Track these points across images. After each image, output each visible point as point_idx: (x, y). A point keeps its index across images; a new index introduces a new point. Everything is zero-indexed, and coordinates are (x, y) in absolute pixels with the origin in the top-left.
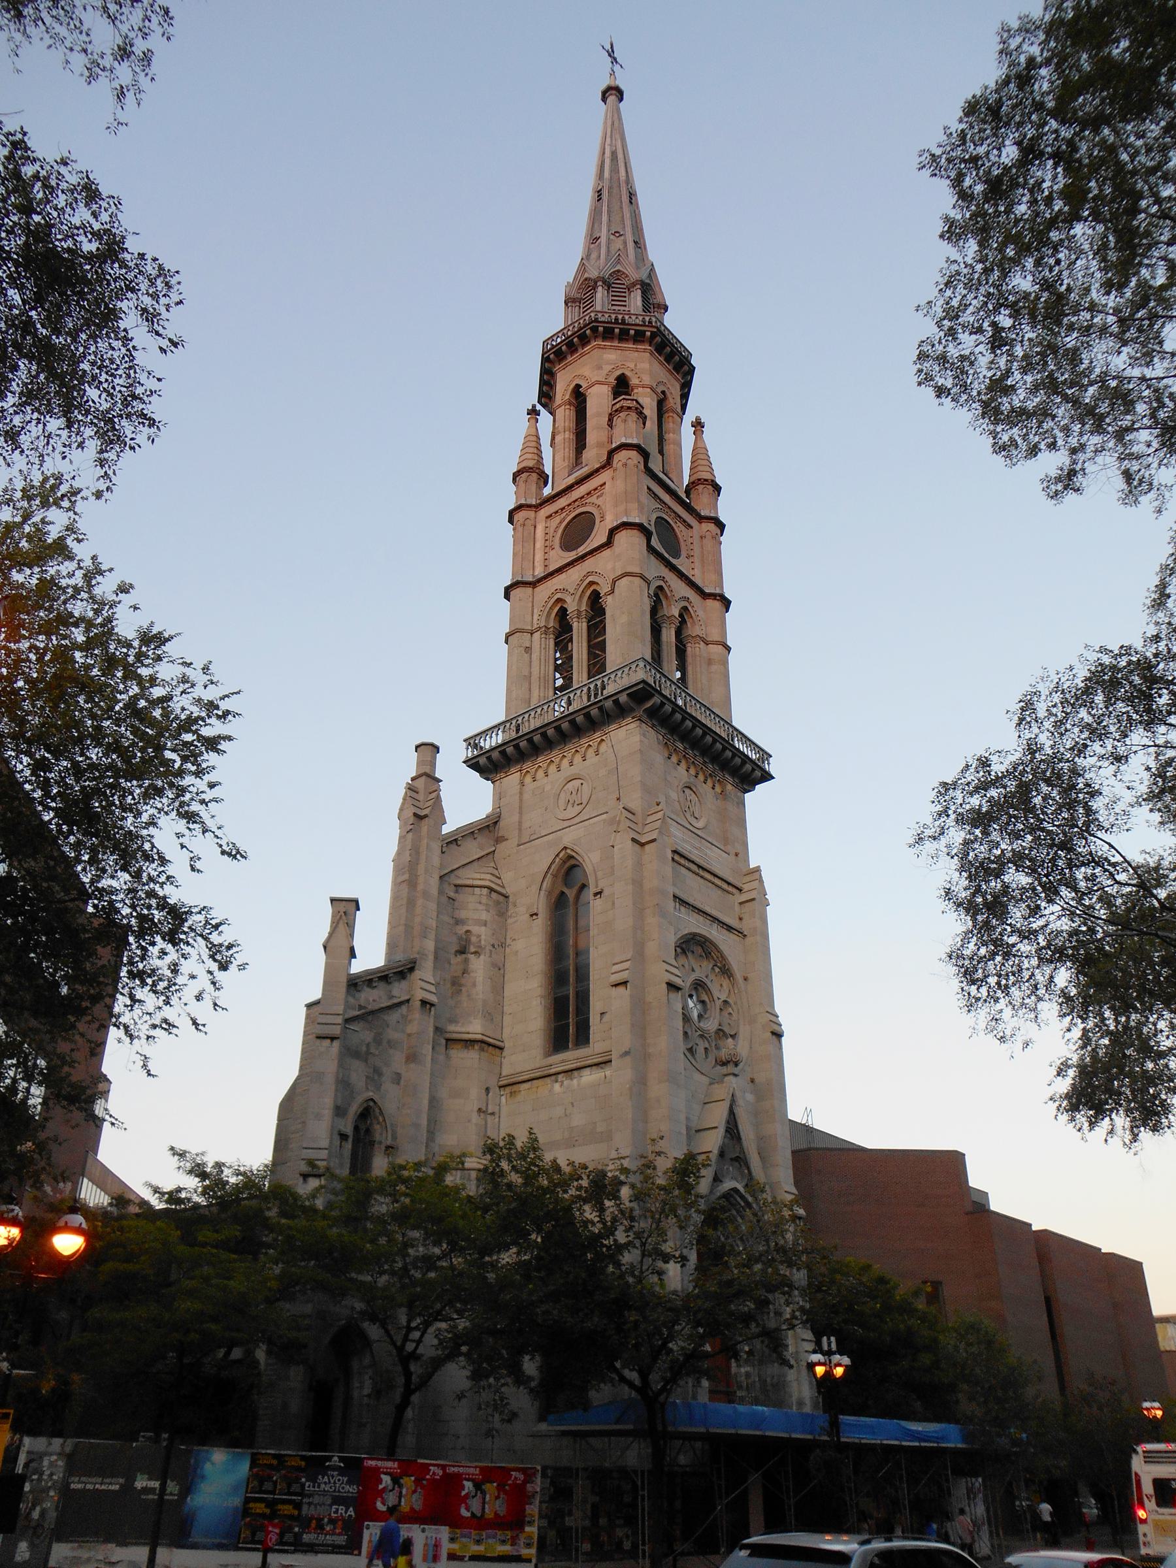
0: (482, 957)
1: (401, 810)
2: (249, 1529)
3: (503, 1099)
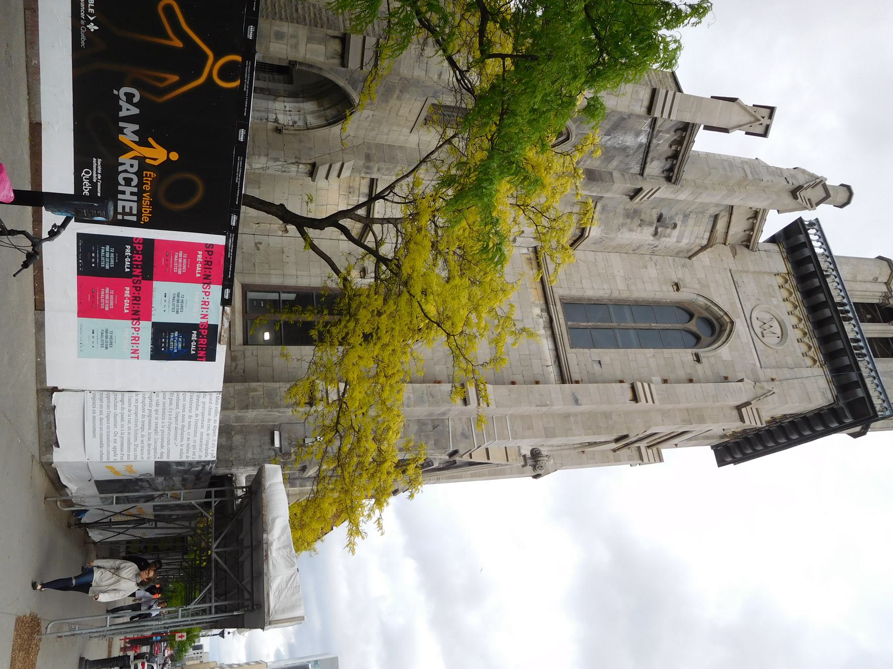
0: (652, 238)
1: (804, 172)
2: (71, 579)
3: (525, 251)
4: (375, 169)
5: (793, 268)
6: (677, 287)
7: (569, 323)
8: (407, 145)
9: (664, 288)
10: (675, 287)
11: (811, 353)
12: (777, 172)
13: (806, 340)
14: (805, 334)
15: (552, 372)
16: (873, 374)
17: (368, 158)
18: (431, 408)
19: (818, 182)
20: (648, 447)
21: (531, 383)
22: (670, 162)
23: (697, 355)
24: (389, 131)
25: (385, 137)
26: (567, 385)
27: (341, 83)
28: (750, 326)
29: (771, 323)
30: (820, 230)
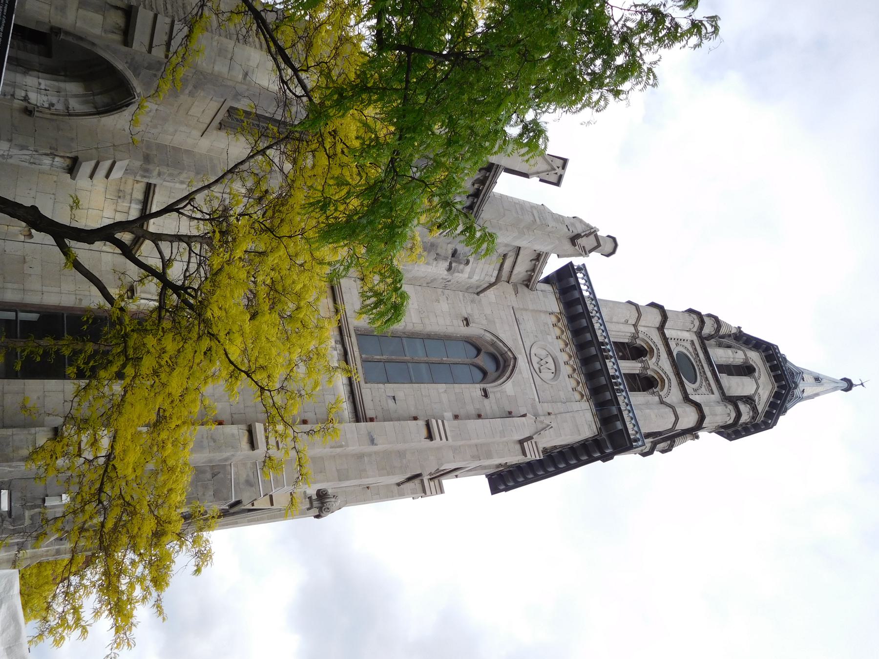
0: (446, 272)
1: (581, 221)
4: (155, 173)
5: (564, 308)
6: (467, 322)
7: (363, 356)
8: (196, 150)
9: (455, 322)
11: (579, 388)
12: (559, 219)
13: (575, 376)
14: (574, 370)
15: (346, 408)
16: (629, 408)
17: (147, 159)
18: (212, 455)
19: (592, 232)
20: (431, 479)
22: (471, 199)
23: (485, 391)
24: (176, 131)
25: (170, 137)
26: (362, 424)
27: (120, 65)
28: (530, 362)
29: (547, 360)
30: (586, 275)
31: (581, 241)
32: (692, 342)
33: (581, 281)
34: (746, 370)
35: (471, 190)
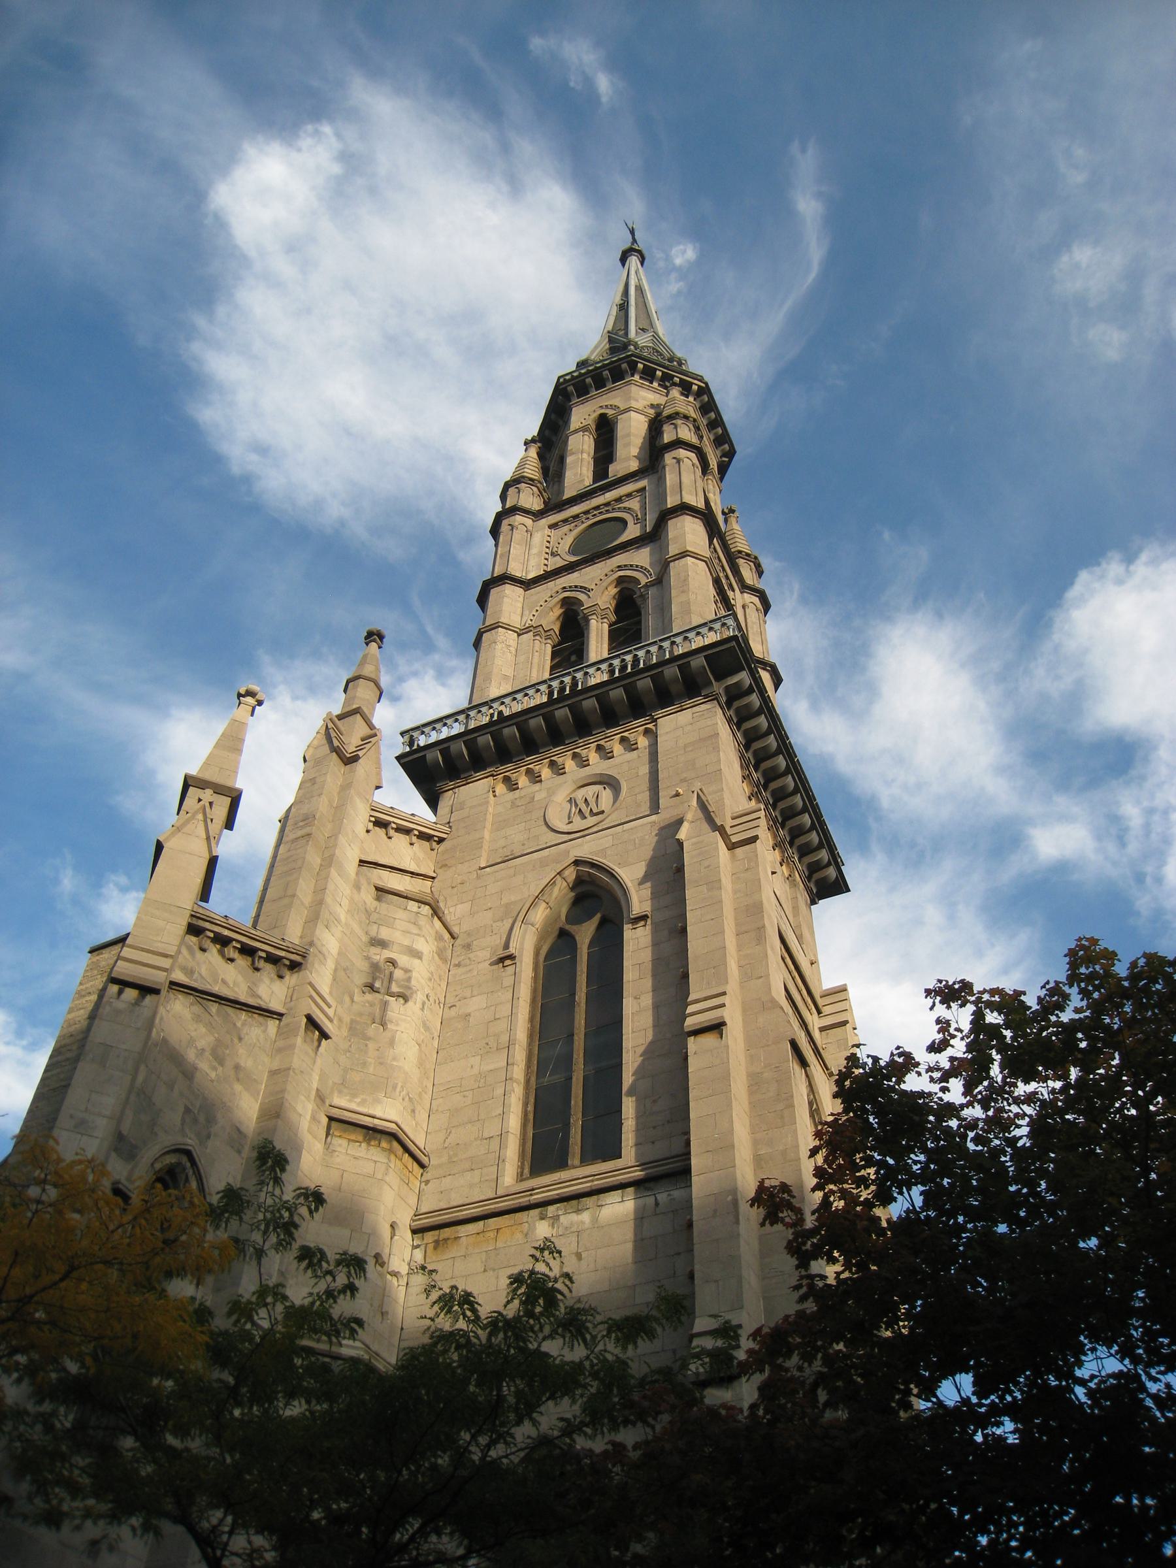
10: (508, 962)
21: (690, 1239)
28: (583, 833)
31: (351, 744)
32: (550, 527)
33: (434, 737)
34: (605, 430)
35: (242, 962)
